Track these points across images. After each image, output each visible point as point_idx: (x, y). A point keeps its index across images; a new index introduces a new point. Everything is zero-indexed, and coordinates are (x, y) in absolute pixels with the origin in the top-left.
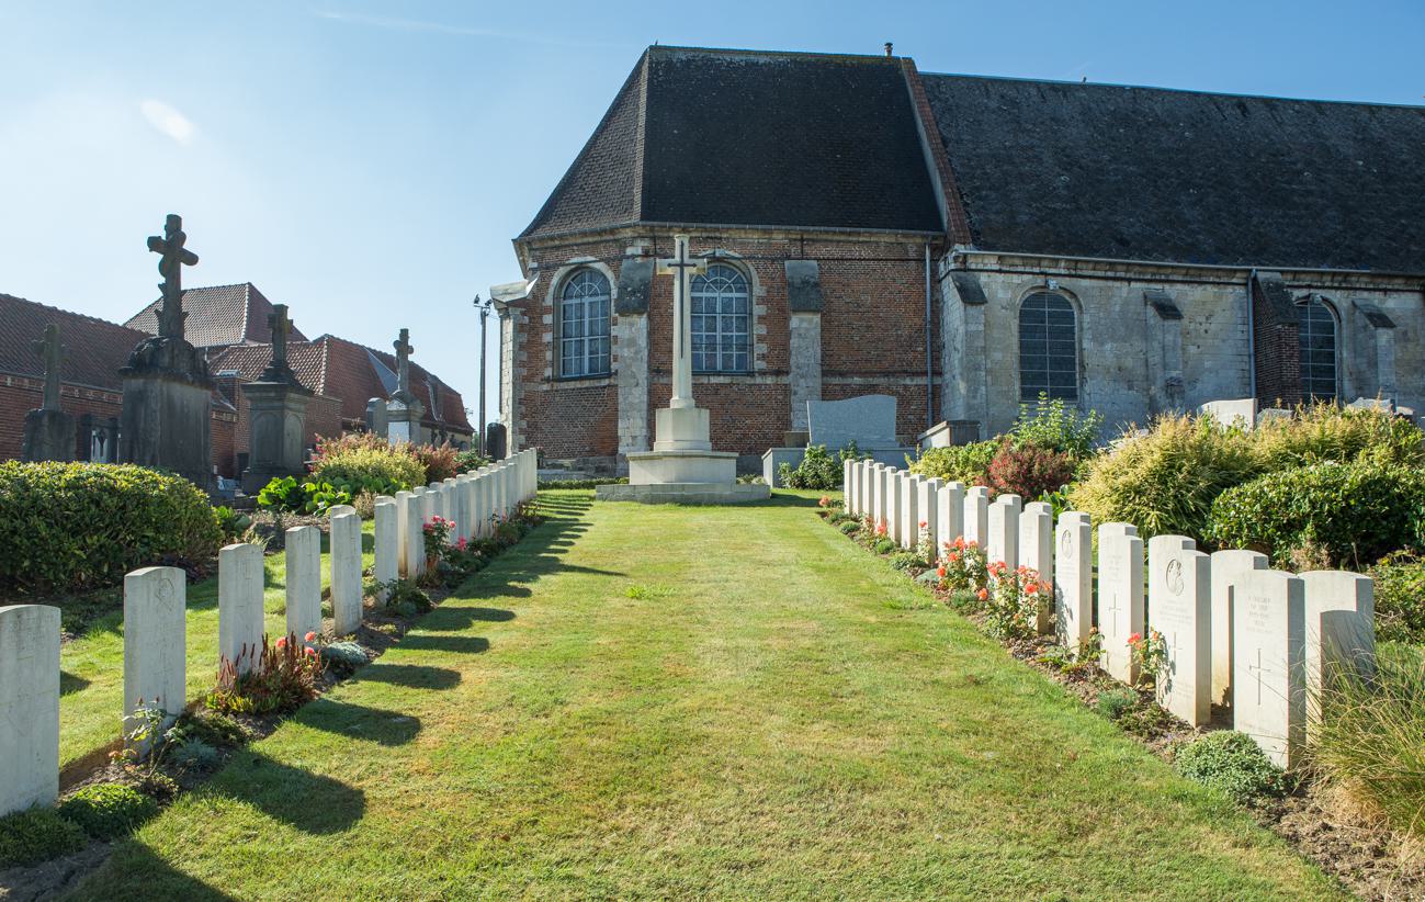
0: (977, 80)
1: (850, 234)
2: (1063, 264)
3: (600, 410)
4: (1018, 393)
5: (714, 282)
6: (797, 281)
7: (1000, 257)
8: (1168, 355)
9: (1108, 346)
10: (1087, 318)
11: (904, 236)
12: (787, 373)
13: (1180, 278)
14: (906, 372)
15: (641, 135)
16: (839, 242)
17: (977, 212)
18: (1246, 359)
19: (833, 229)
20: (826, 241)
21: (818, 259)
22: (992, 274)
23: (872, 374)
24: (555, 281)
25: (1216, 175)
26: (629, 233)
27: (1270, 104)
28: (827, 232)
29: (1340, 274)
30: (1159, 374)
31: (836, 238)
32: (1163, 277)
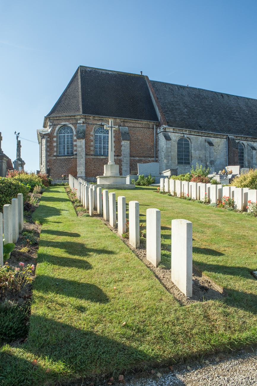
0: (163, 83)
1: (136, 121)
2: (188, 131)
3: (70, 164)
4: (177, 163)
5: (101, 131)
6: (123, 132)
7: (174, 129)
8: (211, 154)
9: (197, 152)
10: (192, 145)
11: (149, 122)
12: (120, 156)
13: (213, 136)
14: (149, 156)
15: (80, 90)
16: (133, 122)
17: (167, 117)
18: (226, 156)
19: (132, 119)
20: (130, 122)
21: (128, 127)
22: (172, 133)
23: (141, 157)
24: (57, 129)
25: (218, 112)
26: (79, 117)
27: (228, 95)
28: (130, 120)
29: (245, 137)
30: (209, 159)
31: (132, 121)
32: (209, 136)
